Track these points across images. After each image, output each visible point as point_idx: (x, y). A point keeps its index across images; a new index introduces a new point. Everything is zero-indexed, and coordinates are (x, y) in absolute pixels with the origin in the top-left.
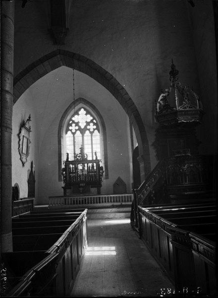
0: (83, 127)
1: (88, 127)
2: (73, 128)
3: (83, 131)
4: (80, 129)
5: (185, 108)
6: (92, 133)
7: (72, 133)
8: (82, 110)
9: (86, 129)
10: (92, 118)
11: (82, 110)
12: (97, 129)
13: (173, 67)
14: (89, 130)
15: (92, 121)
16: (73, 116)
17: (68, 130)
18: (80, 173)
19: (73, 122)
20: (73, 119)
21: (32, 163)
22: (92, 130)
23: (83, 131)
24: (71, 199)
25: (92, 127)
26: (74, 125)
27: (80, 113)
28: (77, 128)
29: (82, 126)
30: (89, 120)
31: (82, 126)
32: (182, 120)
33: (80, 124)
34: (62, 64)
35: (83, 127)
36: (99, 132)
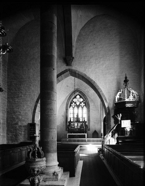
0: (78, 104)
1: (81, 105)
2: (73, 104)
5: (130, 100)
6: (82, 108)
8: (78, 96)
10: (82, 100)
11: (78, 96)
12: (85, 105)
13: (126, 78)
15: (83, 102)
16: (73, 99)
17: (70, 106)
19: (73, 102)
20: (74, 100)
22: (73, 106)
25: (83, 104)
26: (74, 103)
29: (78, 104)
30: (81, 101)
31: (78, 104)
32: (128, 105)
33: (77, 103)
35: (78, 104)
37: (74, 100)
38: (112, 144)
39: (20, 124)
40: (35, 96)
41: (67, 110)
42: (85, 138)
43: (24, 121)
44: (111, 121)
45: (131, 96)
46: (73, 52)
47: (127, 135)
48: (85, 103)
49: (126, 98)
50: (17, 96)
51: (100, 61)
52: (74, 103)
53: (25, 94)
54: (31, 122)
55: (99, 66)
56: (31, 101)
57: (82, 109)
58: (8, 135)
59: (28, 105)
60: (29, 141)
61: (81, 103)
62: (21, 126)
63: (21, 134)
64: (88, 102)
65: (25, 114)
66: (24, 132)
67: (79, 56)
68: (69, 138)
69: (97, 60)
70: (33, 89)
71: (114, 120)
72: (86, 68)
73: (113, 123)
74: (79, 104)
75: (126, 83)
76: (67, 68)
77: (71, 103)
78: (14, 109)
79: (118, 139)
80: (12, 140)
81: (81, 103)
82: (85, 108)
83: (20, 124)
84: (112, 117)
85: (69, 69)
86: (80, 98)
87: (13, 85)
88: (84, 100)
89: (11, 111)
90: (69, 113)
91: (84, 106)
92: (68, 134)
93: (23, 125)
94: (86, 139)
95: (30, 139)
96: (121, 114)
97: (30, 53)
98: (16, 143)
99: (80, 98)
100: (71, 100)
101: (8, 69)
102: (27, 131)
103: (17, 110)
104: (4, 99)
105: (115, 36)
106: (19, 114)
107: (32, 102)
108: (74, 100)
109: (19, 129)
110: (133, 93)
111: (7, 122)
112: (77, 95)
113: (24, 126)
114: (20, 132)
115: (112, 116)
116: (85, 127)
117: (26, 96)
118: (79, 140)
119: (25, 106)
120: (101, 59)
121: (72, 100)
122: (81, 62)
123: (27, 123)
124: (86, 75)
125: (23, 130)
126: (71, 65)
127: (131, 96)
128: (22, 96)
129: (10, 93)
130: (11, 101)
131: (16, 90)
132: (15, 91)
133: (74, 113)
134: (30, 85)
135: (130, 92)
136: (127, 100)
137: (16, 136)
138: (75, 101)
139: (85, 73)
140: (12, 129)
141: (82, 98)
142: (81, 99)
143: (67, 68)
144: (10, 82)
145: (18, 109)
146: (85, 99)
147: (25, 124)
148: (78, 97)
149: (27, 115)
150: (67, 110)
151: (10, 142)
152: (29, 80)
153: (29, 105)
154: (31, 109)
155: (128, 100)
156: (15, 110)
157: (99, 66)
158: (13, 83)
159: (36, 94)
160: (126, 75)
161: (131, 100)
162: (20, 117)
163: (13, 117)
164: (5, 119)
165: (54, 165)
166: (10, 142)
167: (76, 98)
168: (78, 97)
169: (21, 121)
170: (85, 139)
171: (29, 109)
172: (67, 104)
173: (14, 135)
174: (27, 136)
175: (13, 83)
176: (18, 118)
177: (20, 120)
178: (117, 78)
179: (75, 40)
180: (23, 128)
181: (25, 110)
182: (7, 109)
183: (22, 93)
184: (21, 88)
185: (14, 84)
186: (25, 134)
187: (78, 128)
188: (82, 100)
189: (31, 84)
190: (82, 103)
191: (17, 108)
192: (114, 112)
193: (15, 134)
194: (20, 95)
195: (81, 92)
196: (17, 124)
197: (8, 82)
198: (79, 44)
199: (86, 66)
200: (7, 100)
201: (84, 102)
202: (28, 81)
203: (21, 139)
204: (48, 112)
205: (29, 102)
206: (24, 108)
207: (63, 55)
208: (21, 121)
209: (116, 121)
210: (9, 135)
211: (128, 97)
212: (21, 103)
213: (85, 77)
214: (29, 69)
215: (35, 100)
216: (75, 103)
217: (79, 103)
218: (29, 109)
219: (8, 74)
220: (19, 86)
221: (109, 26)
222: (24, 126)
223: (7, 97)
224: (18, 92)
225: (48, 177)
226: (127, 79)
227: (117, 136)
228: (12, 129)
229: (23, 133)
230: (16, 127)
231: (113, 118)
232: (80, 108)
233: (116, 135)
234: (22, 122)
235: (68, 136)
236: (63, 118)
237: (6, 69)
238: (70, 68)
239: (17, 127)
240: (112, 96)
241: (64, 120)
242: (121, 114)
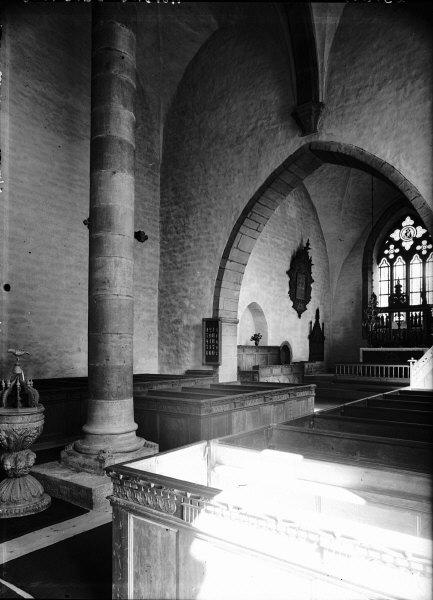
0: (407, 248)
1: (418, 248)
2: (391, 250)
3: (407, 256)
9: (413, 250)
10: (424, 231)
14: (420, 252)
15: (424, 237)
17: (381, 255)
18: (395, 326)
19: (392, 241)
20: (392, 236)
21: (318, 311)
22: (392, 257)
23: (407, 256)
24: (387, 368)
26: (392, 247)
28: (397, 251)
29: (407, 245)
30: (419, 235)
31: (407, 245)
34: (236, 293)
35: (407, 248)
38: (225, 381)
46: (323, 87)
52: (392, 247)
53: (198, 240)
54: (209, 315)
57: (424, 263)
59: (204, 269)
61: (417, 241)
62: (188, 327)
66: (195, 342)
67: (340, 92)
70: (215, 222)
72: (365, 127)
74: (413, 247)
83: (185, 322)
95: (207, 361)
98: (178, 372)
99: (401, 241)
104: (152, 258)
108: (392, 236)
114: (187, 344)
118: (401, 369)
122: (347, 111)
123: (201, 317)
124: (362, 152)
125: (192, 338)
126: (315, 131)
128: (192, 244)
138: (397, 239)
139: (358, 144)
142: (419, 228)
143: (304, 143)
145: (183, 280)
153: (208, 268)
159: (222, 236)
162: (187, 303)
164: (153, 311)
165: (112, 431)
171: (207, 278)
176: (182, 306)
177: (187, 311)
179: (328, 46)
180: (192, 332)
183: (190, 237)
186: (196, 349)
187: (402, 327)
188: (420, 231)
191: (181, 278)
196: (178, 322)
197: (161, 215)
198: (339, 53)
199: (361, 121)
200: (159, 261)
206: (196, 279)
213: (359, 157)
215: (219, 251)
216: (398, 244)
217: (412, 243)
218: (207, 278)
219: (161, 194)
222: (195, 327)
223: (159, 253)
225: (87, 461)
229: (192, 345)
232: (416, 260)
238: (313, 140)
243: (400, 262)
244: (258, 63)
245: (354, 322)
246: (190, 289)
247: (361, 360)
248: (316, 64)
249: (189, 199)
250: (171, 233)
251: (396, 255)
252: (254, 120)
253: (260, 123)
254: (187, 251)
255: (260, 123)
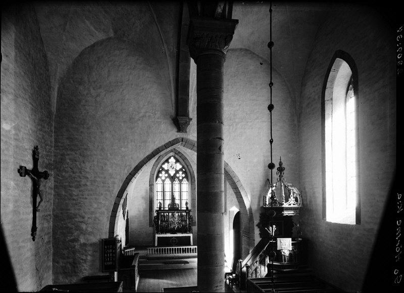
0: (172, 175)
1: (178, 175)
2: (163, 175)
4: (169, 176)
5: (290, 205)
6: (181, 181)
7: (179, 180)
8: (172, 158)
10: (181, 167)
11: (172, 158)
12: (186, 177)
15: (181, 170)
16: (163, 163)
17: (158, 177)
19: (163, 169)
20: (163, 166)
23: (173, 179)
26: (163, 172)
27: (170, 161)
29: (172, 173)
30: (178, 169)
31: (172, 173)
32: (286, 213)
33: (170, 172)
36: (188, 180)
37: (165, 166)
39: (82, 241)
40: (116, 185)
41: (151, 185)
42: (190, 245)
43: (91, 233)
44: (255, 233)
45: (292, 198)
47: (285, 262)
48: (185, 172)
49: (284, 201)
50: (76, 183)
51: (236, 129)
52: (163, 172)
53: (95, 181)
54: (105, 236)
55: (235, 136)
56: (106, 194)
58: (57, 264)
60: (102, 274)
61: (177, 172)
62: (85, 244)
63: (85, 261)
64: (191, 171)
65: (95, 220)
66: (92, 256)
68: (159, 245)
69: (231, 127)
70: (110, 171)
71: (260, 230)
73: (259, 236)
74: (175, 175)
75: (281, 173)
76: (180, 135)
77: (159, 172)
78: (69, 210)
79: (269, 266)
80: (65, 273)
81: (177, 172)
82: (185, 182)
83: (82, 241)
84: (257, 225)
85: (183, 139)
86: (176, 163)
87: (68, 161)
88: (183, 167)
89: (62, 213)
90: (155, 190)
91: (183, 178)
92: (157, 236)
93: (90, 242)
94: (192, 247)
96: (274, 226)
97: (105, 100)
99: (176, 163)
100: (159, 166)
101: (55, 127)
102: (98, 255)
103: (77, 212)
105: (260, 89)
106: (82, 220)
107: (108, 197)
108: (163, 166)
109: (81, 250)
110: (294, 193)
111: (54, 238)
112: (170, 158)
113: (91, 245)
114: (84, 257)
115: (257, 224)
116: (189, 221)
117: (96, 184)
119: (94, 204)
120: (239, 126)
121: (161, 167)
123: (98, 237)
126: (186, 132)
127: (292, 198)
128: (88, 184)
129: (60, 178)
130: (64, 193)
131: (73, 173)
132: (71, 174)
133: (164, 192)
134: (106, 164)
135: (289, 191)
136: (285, 205)
137: (75, 264)
138: (166, 169)
140: (65, 252)
141: (181, 164)
142: (178, 164)
143: (178, 136)
144: (62, 155)
146: (187, 166)
147: (94, 239)
148: (172, 160)
149: (98, 221)
150: (151, 185)
151: (61, 278)
152: (103, 154)
154: (107, 210)
155: (287, 206)
156: (73, 212)
157: (235, 136)
158: (67, 157)
159: (116, 181)
160: (280, 160)
161: (292, 206)
162: (84, 226)
163: (67, 227)
166: (61, 278)
167: (168, 163)
168: (172, 160)
169: (85, 234)
170: (189, 247)
172: (152, 175)
173: (70, 263)
174: (98, 263)
175: (67, 157)
176: (78, 228)
177: (83, 232)
178: (264, 160)
180: (89, 248)
181: (92, 213)
182: (54, 210)
184: (86, 168)
185: (70, 159)
186: (93, 261)
188: (179, 166)
189: (106, 161)
190: (181, 173)
192: (260, 217)
193: (71, 260)
194: (83, 183)
195: (179, 152)
196: (76, 240)
201: (184, 170)
202: (101, 155)
203: (86, 270)
204: (217, 287)
205: (102, 197)
207: (172, 111)
208: (85, 234)
209: (264, 235)
210: (58, 263)
211: (287, 201)
212: (86, 198)
214: (102, 132)
215: (114, 192)
216: (167, 172)
217: (174, 172)
218: (103, 209)
220: (80, 164)
221: (251, 70)
222: (93, 245)
224: (79, 177)
226: (283, 166)
227: (268, 262)
228: (65, 252)
229: (89, 258)
230: (74, 247)
231: (259, 227)
232: (177, 182)
233: (267, 261)
234: (88, 236)
235: (156, 238)
236: (143, 201)
237: (53, 128)
239: (77, 247)
240: (256, 190)
241: (145, 205)
242: (274, 226)
243: (168, 181)
244: (147, 75)
245: (144, 216)
246: (87, 216)
247: (156, 245)
248: (189, 96)
249: (86, 149)
250: (66, 172)
251: (166, 178)
252: (143, 111)
253: (147, 114)
254: (82, 188)
255: (147, 114)
